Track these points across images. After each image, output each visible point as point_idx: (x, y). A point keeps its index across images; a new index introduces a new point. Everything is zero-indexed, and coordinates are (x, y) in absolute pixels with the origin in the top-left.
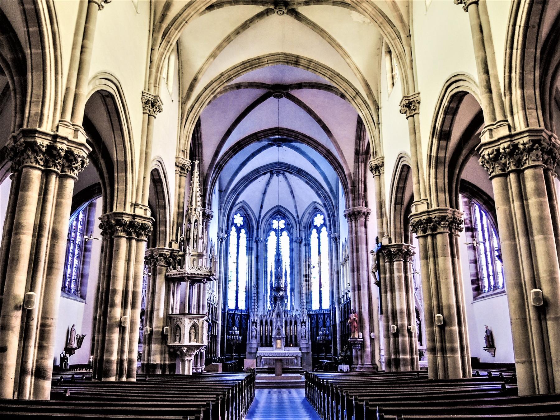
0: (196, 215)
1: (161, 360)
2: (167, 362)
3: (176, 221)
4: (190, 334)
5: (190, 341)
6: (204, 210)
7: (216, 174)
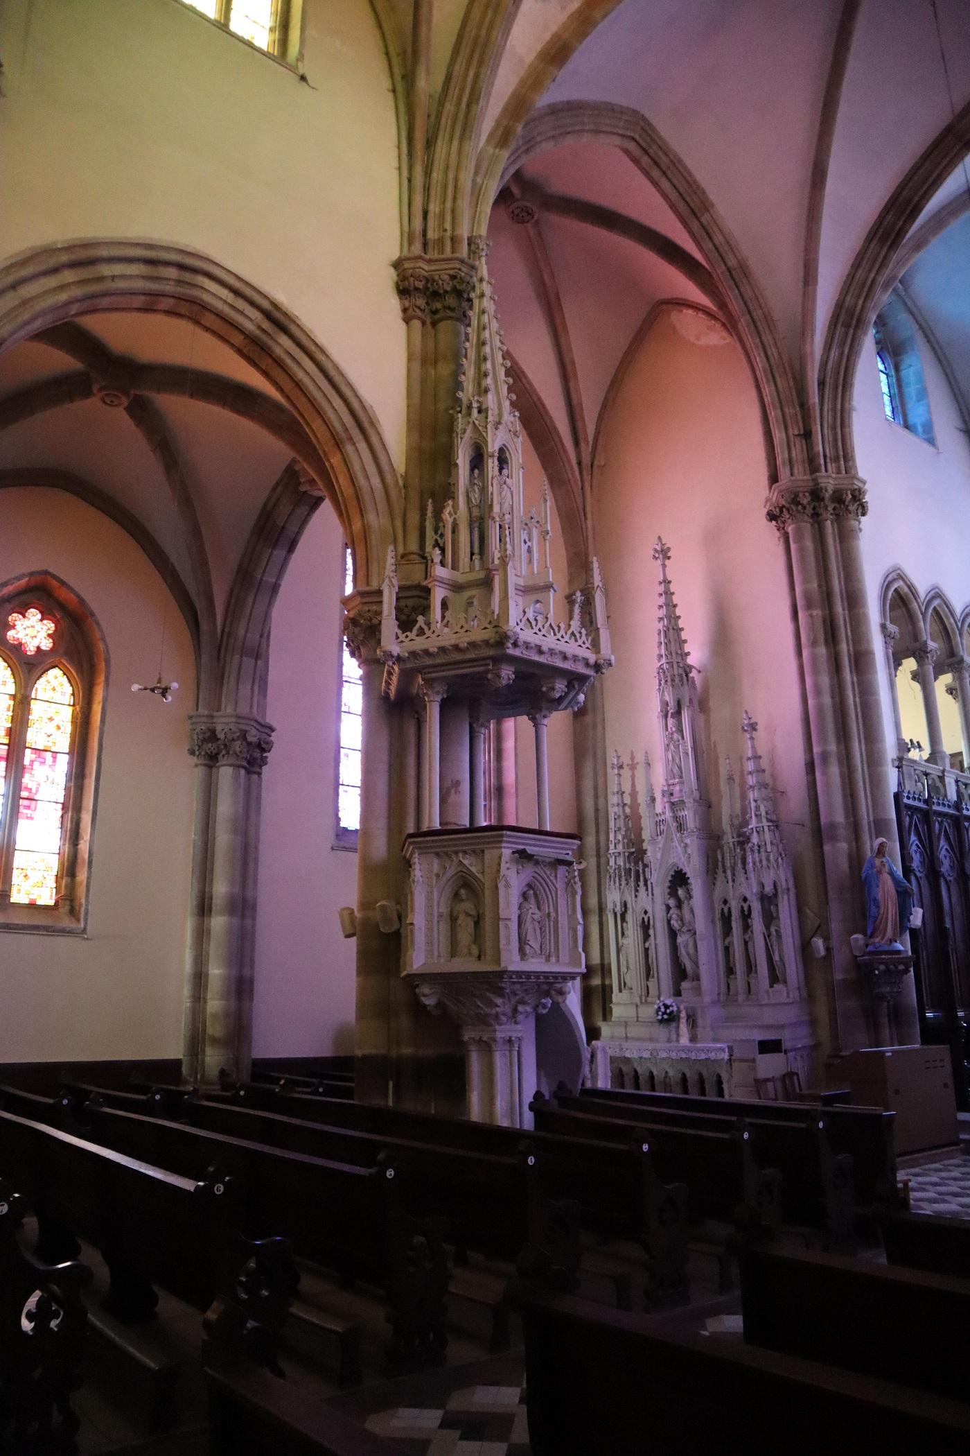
0: (469, 429)
2: (407, 1051)
4: (453, 919)
5: (454, 952)
7: (843, 345)
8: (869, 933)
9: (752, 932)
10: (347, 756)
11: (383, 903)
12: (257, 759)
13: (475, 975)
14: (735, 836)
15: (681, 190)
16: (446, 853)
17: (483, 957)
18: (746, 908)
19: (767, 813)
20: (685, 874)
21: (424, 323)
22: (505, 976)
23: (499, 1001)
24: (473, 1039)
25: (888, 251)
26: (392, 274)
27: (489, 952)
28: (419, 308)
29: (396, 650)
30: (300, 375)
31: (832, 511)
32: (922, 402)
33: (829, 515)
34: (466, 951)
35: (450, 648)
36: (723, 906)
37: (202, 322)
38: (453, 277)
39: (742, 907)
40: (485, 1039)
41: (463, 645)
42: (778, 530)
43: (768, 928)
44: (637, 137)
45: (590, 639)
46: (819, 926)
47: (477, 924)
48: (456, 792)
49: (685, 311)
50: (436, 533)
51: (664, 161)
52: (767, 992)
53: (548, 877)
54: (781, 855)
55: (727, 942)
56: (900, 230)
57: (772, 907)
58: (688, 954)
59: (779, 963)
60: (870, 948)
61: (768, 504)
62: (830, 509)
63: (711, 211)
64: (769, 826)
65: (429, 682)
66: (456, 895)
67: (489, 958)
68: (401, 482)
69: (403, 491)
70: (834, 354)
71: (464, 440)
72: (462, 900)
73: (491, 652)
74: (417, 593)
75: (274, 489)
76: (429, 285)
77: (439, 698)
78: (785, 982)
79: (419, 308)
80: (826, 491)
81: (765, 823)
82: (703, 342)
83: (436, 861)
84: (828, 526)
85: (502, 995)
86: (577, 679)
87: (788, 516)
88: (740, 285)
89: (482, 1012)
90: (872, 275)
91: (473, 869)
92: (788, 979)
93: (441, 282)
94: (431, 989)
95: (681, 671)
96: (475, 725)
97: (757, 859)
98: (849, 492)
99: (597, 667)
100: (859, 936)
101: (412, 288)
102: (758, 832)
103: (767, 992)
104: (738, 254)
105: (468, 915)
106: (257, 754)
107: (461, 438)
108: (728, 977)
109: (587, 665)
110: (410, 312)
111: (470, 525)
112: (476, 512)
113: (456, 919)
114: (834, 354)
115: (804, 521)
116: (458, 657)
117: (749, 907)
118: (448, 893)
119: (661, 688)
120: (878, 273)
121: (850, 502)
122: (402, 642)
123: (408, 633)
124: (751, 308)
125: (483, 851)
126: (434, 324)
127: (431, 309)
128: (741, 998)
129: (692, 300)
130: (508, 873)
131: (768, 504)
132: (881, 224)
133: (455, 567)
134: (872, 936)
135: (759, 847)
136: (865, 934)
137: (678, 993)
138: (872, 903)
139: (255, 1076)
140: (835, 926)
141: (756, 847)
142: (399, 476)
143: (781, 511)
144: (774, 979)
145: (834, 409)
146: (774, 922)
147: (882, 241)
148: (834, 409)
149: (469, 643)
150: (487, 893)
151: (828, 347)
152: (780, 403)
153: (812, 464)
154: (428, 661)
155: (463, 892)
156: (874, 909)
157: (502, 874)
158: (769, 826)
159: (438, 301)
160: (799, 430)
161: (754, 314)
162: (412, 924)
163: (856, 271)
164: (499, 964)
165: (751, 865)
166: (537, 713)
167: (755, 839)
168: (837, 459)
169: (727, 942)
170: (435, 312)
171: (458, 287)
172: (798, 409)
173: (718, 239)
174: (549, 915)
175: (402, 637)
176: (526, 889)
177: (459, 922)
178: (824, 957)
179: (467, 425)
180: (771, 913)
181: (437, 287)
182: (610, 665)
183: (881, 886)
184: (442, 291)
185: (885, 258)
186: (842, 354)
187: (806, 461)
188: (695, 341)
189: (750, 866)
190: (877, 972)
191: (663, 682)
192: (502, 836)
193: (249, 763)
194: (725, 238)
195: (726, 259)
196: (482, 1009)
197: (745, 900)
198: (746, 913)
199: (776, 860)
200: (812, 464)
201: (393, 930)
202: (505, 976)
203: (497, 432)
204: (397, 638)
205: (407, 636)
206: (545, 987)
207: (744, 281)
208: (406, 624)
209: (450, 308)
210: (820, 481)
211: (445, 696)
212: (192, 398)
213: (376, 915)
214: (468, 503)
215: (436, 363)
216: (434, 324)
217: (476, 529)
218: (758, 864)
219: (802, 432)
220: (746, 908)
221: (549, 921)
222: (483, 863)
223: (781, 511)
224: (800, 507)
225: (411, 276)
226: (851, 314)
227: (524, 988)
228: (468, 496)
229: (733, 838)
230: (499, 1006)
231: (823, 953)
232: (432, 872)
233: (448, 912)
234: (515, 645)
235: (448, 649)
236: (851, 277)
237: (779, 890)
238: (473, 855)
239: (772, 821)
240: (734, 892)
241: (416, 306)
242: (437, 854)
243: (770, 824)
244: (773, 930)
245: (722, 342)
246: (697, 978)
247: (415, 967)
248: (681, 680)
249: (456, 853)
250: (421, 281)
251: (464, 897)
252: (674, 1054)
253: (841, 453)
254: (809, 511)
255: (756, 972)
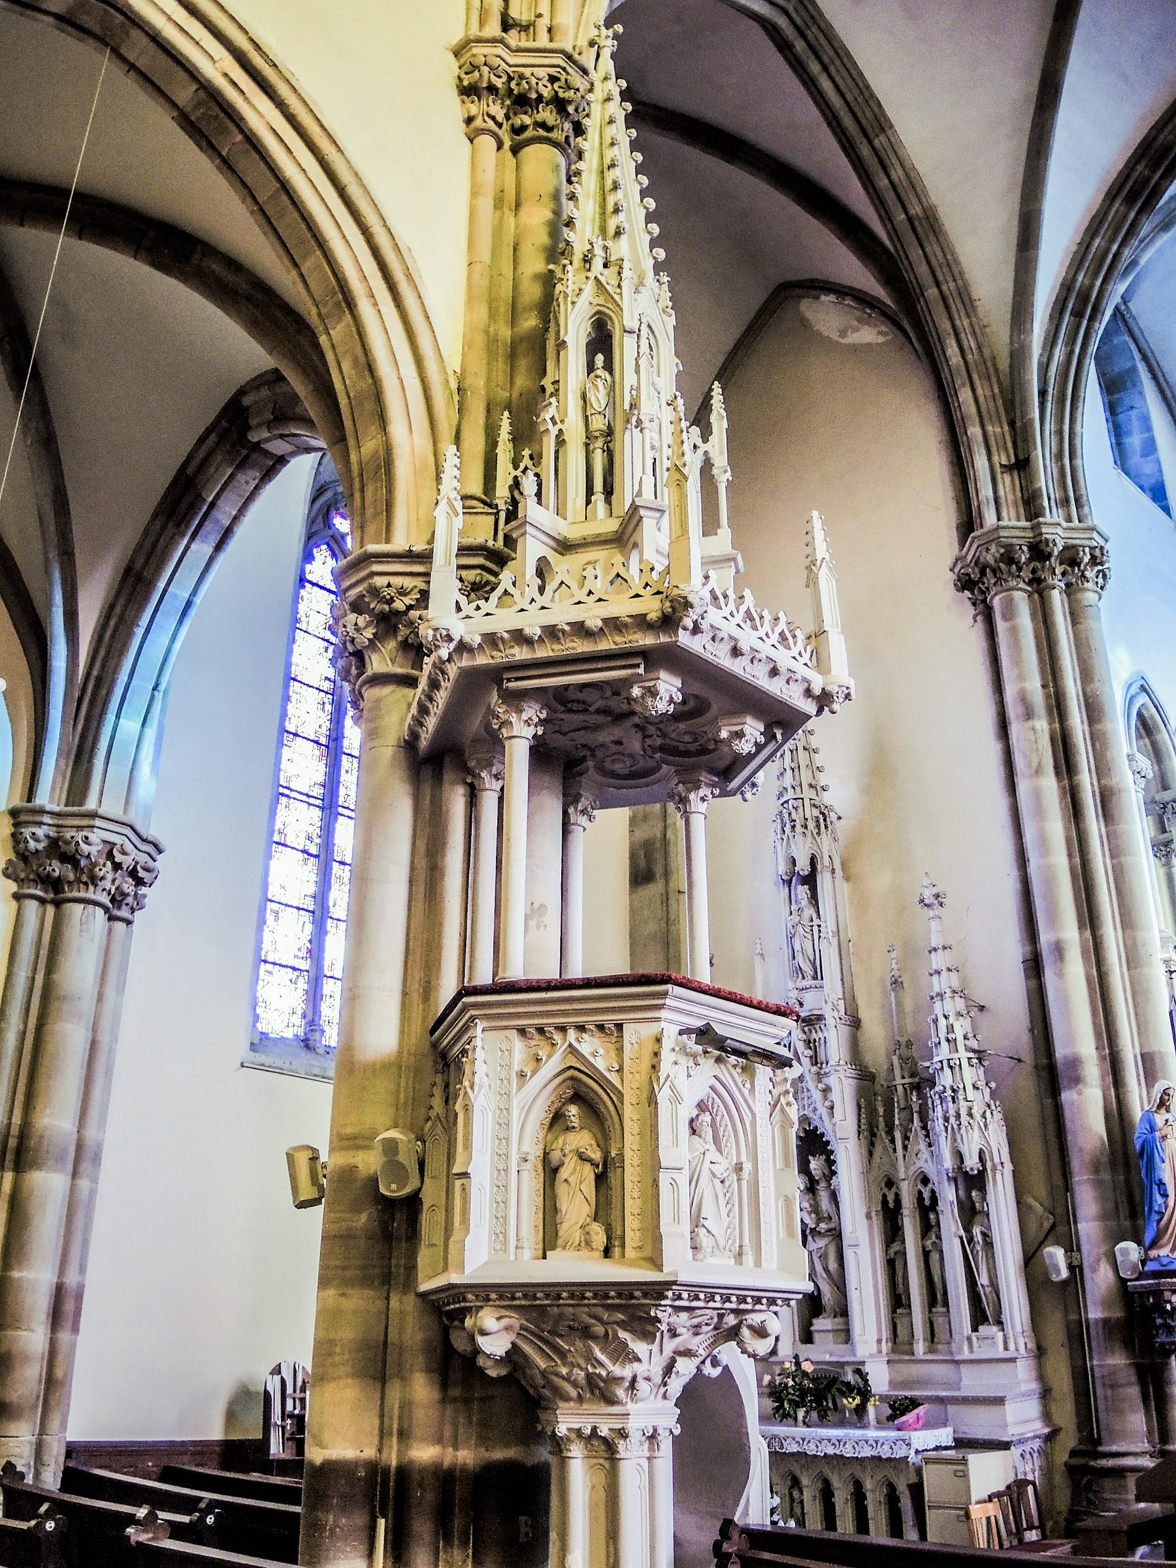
0: (589, 288)
1: (383, 1434)
2: (424, 1453)
3: (478, 382)
4: (551, 1171)
5: (550, 1240)
6: (1036, 528)
8: (1147, 1241)
9: (939, 1237)
10: (276, 914)
11: (393, 1134)
12: (127, 895)
13: (601, 1290)
14: (906, 1074)
15: (849, 97)
16: (541, 1030)
17: (617, 1251)
18: (926, 1195)
19: (965, 1038)
20: (823, 1135)
21: (500, 146)
22: (670, 1294)
23: (639, 1347)
24: (579, 1432)
25: (1138, 213)
26: (452, 67)
27: (632, 1237)
28: (493, 118)
29: (459, 629)
30: (289, 169)
31: (1060, 577)
32: (1149, 458)
33: (1056, 581)
34: (577, 1236)
35: (567, 628)
36: (885, 1190)
37: (123, 51)
38: (553, 79)
39: (920, 1193)
40: (604, 1431)
41: (594, 623)
42: (974, 604)
43: (968, 1229)
44: (791, 9)
45: (809, 649)
46: (1053, 1227)
47: (601, 1179)
48: (538, 927)
49: (823, 298)
50: (516, 467)
51: (828, 53)
52: (969, 1339)
53: (740, 1090)
54: (989, 1106)
55: (892, 1252)
56: (1157, 184)
57: (974, 1194)
58: (826, 1270)
59: (988, 1290)
60: (1151, 1266)
61: (959, 566)
62: (1059, 570)
63: (889, 132)
64: (969, 1059)
65: (515, 699)
66: (557, 1119)
67: (630, 1253)
68: (454, 385)
69: (456, 398)
70: (1059, 353)
71: (577, 306)
72: (569, 1129)
73: (646, 640)
74: (481, 561)
75: (201, 440)
76: (513, 85)
77: (529, 732)
78: (999, 1323)
79: (493, 118)
80: (1055, 545)
81: (963, 1054)
82: (853, 338)
83: (518, 1044)
84: (1057, 598)
85: (648, 1336)
86: (779, 724)
87: (993, 581)
88: (926, 244)
89: (604, 1373)
90: (1115, 247)
91: (600, 1064)
92: (1006, 1317)
93: (534, 81)
94: (499, 1319)
95: (816, 812)
96: (571, 810)
97: (952, 1112)
98: (1087, 550)
99: (824, 700)
100: (1130, 1245)
101: (485, 85)
102: (951, 1067)
103: (969, 1339)
104: (924, 200)
105: (582, 1157)
106: (128, 886)
107: (573, 303)
108: (894, 1312)
109: (808, 693)
110: (478, 123)
111: (587, 445)
112: (598, 424)
113: (556, 1170)
114: (1059, 353)
115: (1020, 589)
116: (582, 647)
117: (933, 1192)
118: (540, 1113)
119: (785, 838)
120: (1123, 244)
121: (1087, 564)
122: (468, 617)
123: (482, 603)
124: (941, 278)
125: (619, 1027)
126: (515, 150)
127: (513, 125)
128: (920, 1347)
129: (838, 281)
130: (673, 1070)
131: (959, 566)
132: (1128, 177)
133: (560, 511)
134: (1154, 1244)
135: (954, 1091)
136: (1139, 1243)
137: (807, 1337)
138: (1155, 1187)
139: (73, 1479)
140: (1089, 1228)
141: (949, 1092)
142: (450, 373)
143: (983, 573)
144: (979, 1317)
145: (1060, 432)
146: (978, 1218)
147: (1130, 200)
148: (1060, 432)
149: (605, 621)
150: (630, 1114)
151: (1050, 342)
152: (980, 417)
153: (1031, 505)
154: (520, 654)
155: (573, 1110)
156: (1159, 1200)
157: (662, 1075)
158: (969, 1059)
159: (526, 113)
160: (1009, 460)
161: (944, 287)
162: (465, 1175)
163: (1092, 239)
164: (659, 1267)
165: (941, 1121)
166: (690, 791)
167: (946, 1079)
168: (1065, 502)
169: (892, 1252)
170: (517, 131)
171: (561, 95)
172: (1006, 428)
173: (897, 173)
174: (739, 1168)
175: (468, 609)
176: (695, 1112)
177: (564, 1173)
178: (1064, 1283)
179: (586, 284)
180: (973, 1203)
181: (527, 87)
182: (848, 697)
183: (1167, 1161)
184: (534, 96)
185: (1134, 225)
186: (1072, 352)
187: (1020, 502)
188: (840, 340)
189: (938, 1125)
190: (1168, 1307)
191: (788, 829)
192: (665, 994)
193: (113, 900)
194: (906, 174)
195: (909, 207)
196: (602, 1365)
197: (925, 1180)
198: (927, 1202)
199: (984, 1116)
200: (1031, 505)
201: (407, 1190)
202: (670, 1294)
203: (638, 296)
204: (459, 609)
205: (478, 608)
206: (731, 1320)
207: (932, 238)
208: (478, 590)
209: (543, 125)
210: (1044, 530)
211: (540, 733)
212: (80, 239)
213: (369, 1162)
214: (585, 409)
215: (518, 205)
216: (515, 150)
217: (599, 452)
218: (952, 1120)
219: (1013, 460)
220: (926, 1195)
221: (739, 1180)
222: (620, 1050)
223: (983, 573)
224: (1014, 567)
225: (485, 64)
226: (1084, 297)
227: (695, 1321)
228: (584, 397)
229: (903, 1078)
230: (638, 1360)
231: (1064, 1274)
232: (510, 1066)
233: (540, 1153)
234: (696, 630)
235: (563, 631)
236: (1084, 246)
237: (989, 1165)
238: (598, 1034)
239: (974, 1051)
240: (907, 1169)
241: (489, 115)
242: (522, 1031)
243: (971, 1055)
244: (977, 1231)
245: (881, 339)
246: (843, 1312)
247: (468, 1270)
248: (818, 826)
249: (562, 1029)
250: (500, 77)
251: (575, 1122)
252: (812, 1446)
253: (1071, 494)
254: (1026, 574)
255: (946, 1304)
